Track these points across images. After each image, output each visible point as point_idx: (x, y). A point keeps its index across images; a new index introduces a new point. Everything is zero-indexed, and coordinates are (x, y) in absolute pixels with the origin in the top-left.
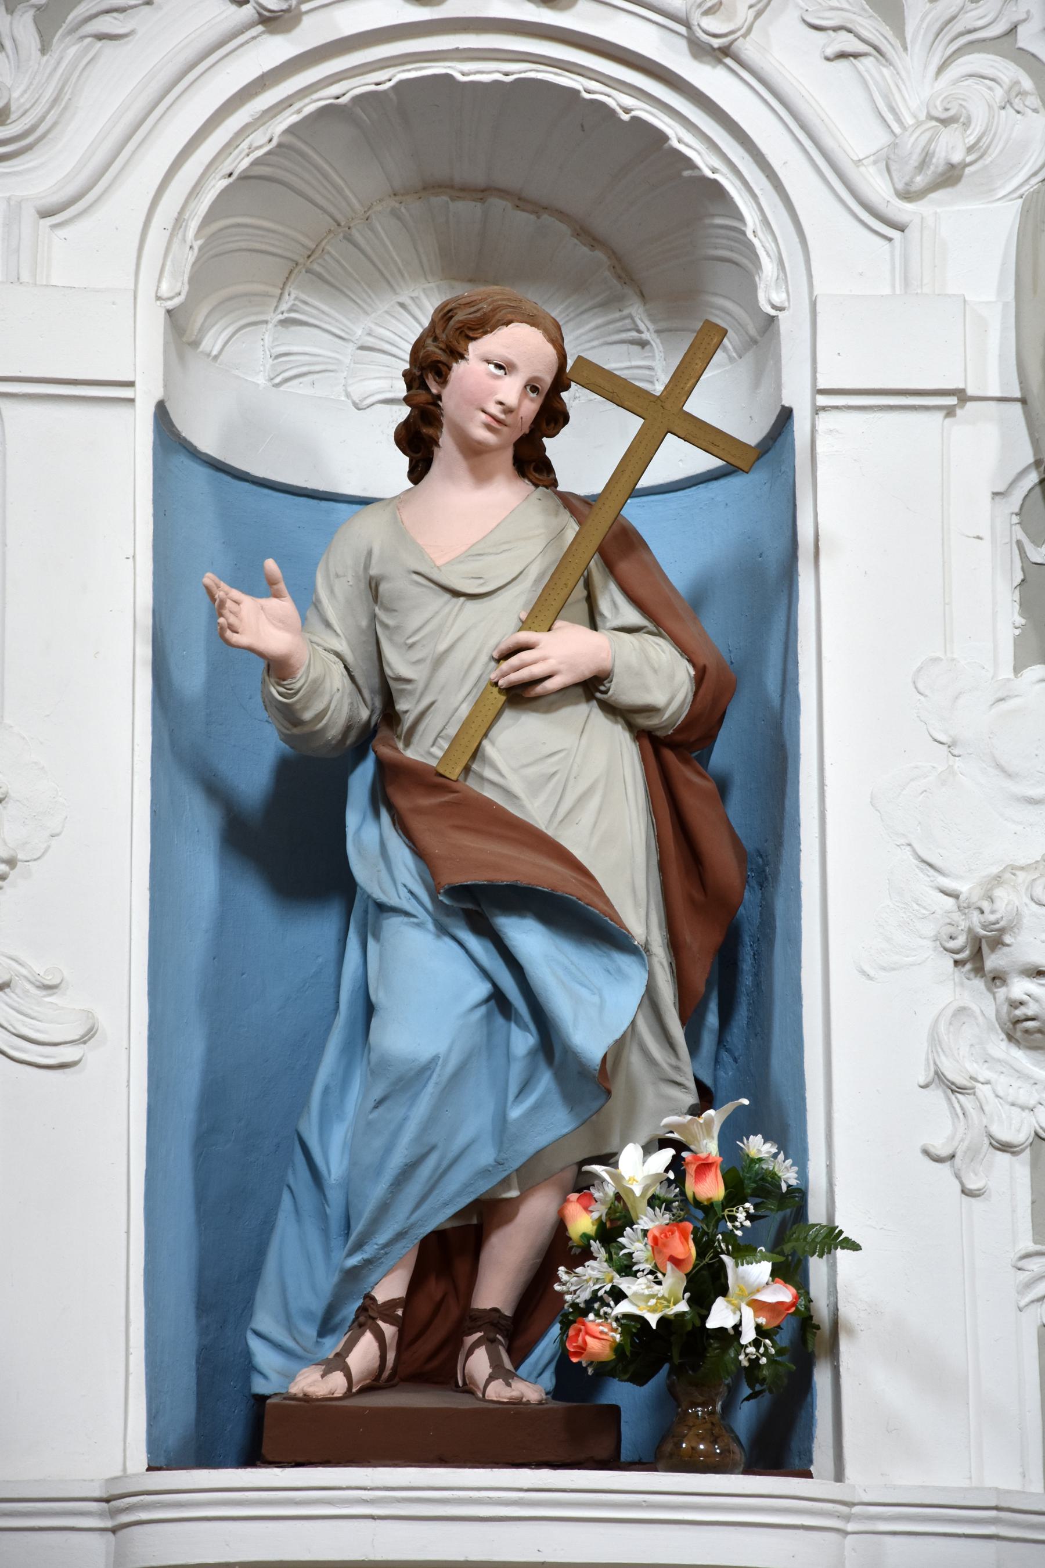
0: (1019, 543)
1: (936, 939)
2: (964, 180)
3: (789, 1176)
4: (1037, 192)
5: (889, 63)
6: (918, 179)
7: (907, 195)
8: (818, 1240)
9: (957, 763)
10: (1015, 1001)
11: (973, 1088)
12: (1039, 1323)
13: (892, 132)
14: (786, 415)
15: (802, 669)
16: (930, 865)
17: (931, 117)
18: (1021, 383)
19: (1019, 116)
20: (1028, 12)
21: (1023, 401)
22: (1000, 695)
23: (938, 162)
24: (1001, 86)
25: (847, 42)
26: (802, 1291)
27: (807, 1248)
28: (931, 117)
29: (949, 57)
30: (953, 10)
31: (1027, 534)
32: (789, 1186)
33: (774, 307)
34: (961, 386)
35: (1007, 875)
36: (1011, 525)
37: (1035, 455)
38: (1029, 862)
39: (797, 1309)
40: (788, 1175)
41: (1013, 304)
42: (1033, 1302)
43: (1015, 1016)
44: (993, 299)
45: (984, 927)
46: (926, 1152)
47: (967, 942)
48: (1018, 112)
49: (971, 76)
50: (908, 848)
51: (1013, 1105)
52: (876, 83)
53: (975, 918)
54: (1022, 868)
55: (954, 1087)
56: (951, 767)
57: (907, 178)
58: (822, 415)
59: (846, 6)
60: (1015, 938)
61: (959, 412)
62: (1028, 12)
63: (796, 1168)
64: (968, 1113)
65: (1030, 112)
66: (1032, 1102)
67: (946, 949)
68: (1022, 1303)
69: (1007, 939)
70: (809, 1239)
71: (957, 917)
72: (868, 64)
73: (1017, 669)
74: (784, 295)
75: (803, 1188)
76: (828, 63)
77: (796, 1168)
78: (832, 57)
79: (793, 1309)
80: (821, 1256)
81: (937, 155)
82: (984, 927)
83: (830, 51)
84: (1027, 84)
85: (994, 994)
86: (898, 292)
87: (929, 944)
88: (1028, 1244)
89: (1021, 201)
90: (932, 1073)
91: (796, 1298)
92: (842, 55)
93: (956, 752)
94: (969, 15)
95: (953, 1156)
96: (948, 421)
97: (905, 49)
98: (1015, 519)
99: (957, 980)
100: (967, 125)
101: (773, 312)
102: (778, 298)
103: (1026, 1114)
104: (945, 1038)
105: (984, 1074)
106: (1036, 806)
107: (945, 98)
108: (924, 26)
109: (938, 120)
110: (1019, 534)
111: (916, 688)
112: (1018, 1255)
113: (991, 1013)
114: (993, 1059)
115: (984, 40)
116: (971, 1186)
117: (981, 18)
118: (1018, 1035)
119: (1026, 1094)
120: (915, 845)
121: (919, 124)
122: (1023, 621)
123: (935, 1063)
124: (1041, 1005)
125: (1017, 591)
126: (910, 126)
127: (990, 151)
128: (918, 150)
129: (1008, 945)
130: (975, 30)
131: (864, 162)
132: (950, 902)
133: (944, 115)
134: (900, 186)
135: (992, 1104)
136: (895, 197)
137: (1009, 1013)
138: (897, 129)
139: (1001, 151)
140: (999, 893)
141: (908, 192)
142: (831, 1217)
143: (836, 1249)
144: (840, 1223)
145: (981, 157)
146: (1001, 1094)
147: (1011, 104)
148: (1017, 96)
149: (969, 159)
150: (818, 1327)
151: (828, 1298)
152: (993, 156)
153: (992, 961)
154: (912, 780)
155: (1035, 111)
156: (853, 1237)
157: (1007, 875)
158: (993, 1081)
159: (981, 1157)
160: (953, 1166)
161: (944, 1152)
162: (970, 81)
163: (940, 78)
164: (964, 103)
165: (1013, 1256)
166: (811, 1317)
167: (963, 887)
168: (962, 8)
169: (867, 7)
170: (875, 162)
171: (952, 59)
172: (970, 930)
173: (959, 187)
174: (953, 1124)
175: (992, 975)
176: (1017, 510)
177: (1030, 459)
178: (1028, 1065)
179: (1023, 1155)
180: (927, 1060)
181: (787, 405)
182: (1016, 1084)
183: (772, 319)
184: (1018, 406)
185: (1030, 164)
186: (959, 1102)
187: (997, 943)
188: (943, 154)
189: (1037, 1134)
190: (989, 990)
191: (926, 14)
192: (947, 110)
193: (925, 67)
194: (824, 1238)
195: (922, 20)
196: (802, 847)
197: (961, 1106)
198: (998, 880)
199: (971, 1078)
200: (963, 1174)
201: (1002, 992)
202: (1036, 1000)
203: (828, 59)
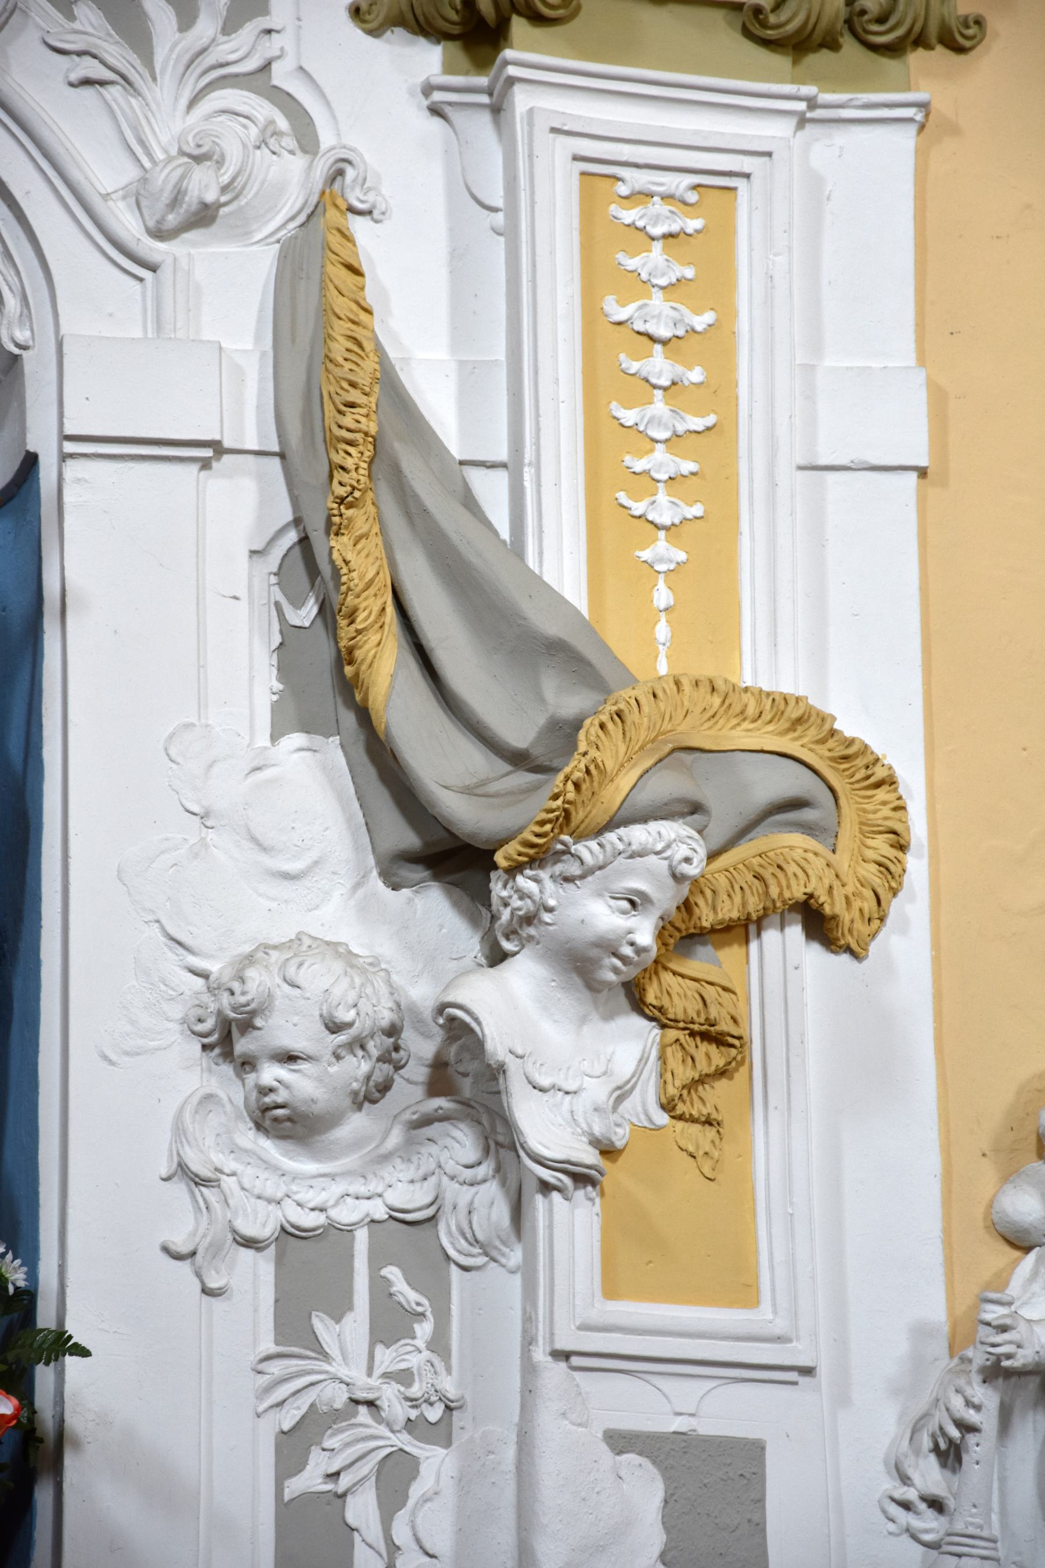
0: (277, 604)
1: (184, 1021)
2: (218, 220)
3: (18, 1277)
4: (295, 238)
5: (138, 93)
6: (170, 217)
7: (159, 234)
8: (45, 1346)
9: (211, 835)
10: (264, 1088)
11: (218, 1180)
12: (277, 1430)
13: (142, 166)
14: (31, 461)
15: (46, 733)
16: (180, 943)
17: (182, 153)
18: (279, 436)
19: (274, 157)
20: (282, 49)
21: (282, 456)
22: (255, 764)
23: (191, 200)
24: (256, 125)
25: (91, 68)
26: (26, 1402)
27: (33, 1356)
28: (182, 153)
29: (201, 91)
30: (205, 41)
31: (285, 595)
32: (16, 1288)
33: (18, 345)
34: (217, 437)
35: (260, 955)
36: (270, 586)
37: (294, 512)
38: (283, 940)
39: (19, 1422)
40: (17, 1276)
41: (271, 354)
42: (272, 1407)
43: (265, 1103)
44: (250, 346)
45: (234, 1009)
46: (165, 1249)
47: (216, 1025)
48: (274, 153)
49: (224, 112)
50: (157, 925)
51: (259, 1197)
52: (124, 114)
53: (225, 999)
54: (275, 947)
55: (197, 1180)
56: (203, 839)
57: (157, 217)
58: (70, 462)
59: (90, 30)
60: (266, 1021)
61: (215, 464)
62: (282, 49)
63: (25, 1269)
64: (211, 1207)
65: (286, 153)
66: (279, 1195)
67: (194, 1033)
68: (261, 1409)
69: (258, 1022)
70: (35, 1345)
71: (206, 998)
72: (114, 93)
73: (275, 738)
74: (28, 333)
75: (32, 1290)
76: (72, 89)
77: (25, 1269)
78: (76, 82)
79: (14, 1422)
80: (47, 1364)
81: (189, 194)
82: (234, 1009)
83: (74, 77)
84: (283, 124)
85: (243, 1080)
86: (150, 335)
87: (175, 1027)
88: (268, 1345)
89: (278, 246)
90: (175, 1165)
91: (18, 1410)
92: (87, 82)
93: (208, 824)
94: (221, 47)
95: (193, 1254)
96: (203, 473)
97: (154, 79)
98: (274, 579)
99: (204, 1065)
100: (220, 163)
101: (16, 351)
102: (22, 335)
103: (272, 1207)
104: (190, 1127)
105: (230, 1164)
106: (292, 882)
107: (197, 133)
108: (174, 56)
109: (190, 156)
110: (278, 595)
111: (168, 755)
112: (259, 1358)
113: (239, 1099)
114: (241, 1149)
115: (237, 75)
116: (213, 1284)
117: (233, 52)
118: (267, 1123)
119: (272, 1187)
120: (164, 921)
121: (170, 159)
122: (281, 687)
123: (179, 1154)
124: (291, 1092)
125: (275, 655)
126: (161, 161)
127: (245, 192)
128: (169, 187)
129: (259, 1029)
130: (227, 64)
131: (113, 196)
132: (200, 982)
133: (197, 152)
134: (151, 224)
135: (237, 1197)
136: (146, 235)
137: (258, 1100)
138: (147, 164)
139: (257, 194)
140: (251, 973)
141: (159, 231)
142: (61, 1320)
143: (64, 1355)
144: (70, 1327)
145: (236, 198)
146: (247, 1186)
147: (266, 144)
148: (272, 136)
149: (223, 199)
150: (41, 1441)
151: (54, 1408)
152: (249, 197)
153: (242, 1046)
154: (163, 852)
155: (292, 152)
156: (84, 1343)
157: (260, 955)
158: (239, 1172)
159: (224, 1253)
160: (193, 1264)
161: (184, 1249)
162: (223, 118)
163: (192, 112)
164: (216, 140)
165: (253, 1358)
166: (34, 1430)
167: (214, 967)
168: (214, 40)
169: (113, 32)
170: (124, 198)
171: (204, 93)
172: (219, 1013)
173: (214, 228)
174: (196, 1219)
175: (241, 1060)
176: (275, 570)
177: (289, 517)
178: (277, 1155)
179: (266, 1252)
180: (171, 1150)
181: (32, 450)
182: (263, 1175)
183: (16, 358)
184: (277, 461)
185: (284, 211)
186: (202, 1195)
187: (247, 1026)
188: (196, 193)
189: (283, 1228)
190: (238, 1075)
191: (175, 45)
192: (199, 146)
193: (176, 99)
194: (52, 1344)
195: (172, 50)
196: (43, 923)
197: (205, 1200)
198: (249, 959)
199: (216, 1169)
200: (204, 1273)
201: (251, 1078)
202: (287, 1086)
203: (72, 85)
